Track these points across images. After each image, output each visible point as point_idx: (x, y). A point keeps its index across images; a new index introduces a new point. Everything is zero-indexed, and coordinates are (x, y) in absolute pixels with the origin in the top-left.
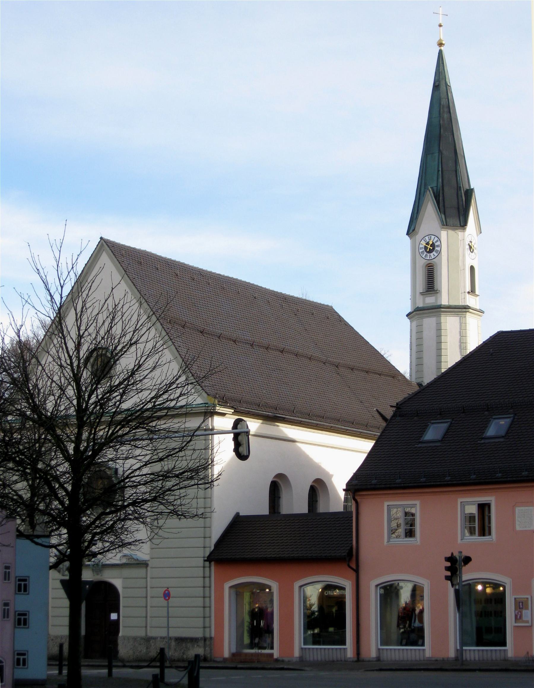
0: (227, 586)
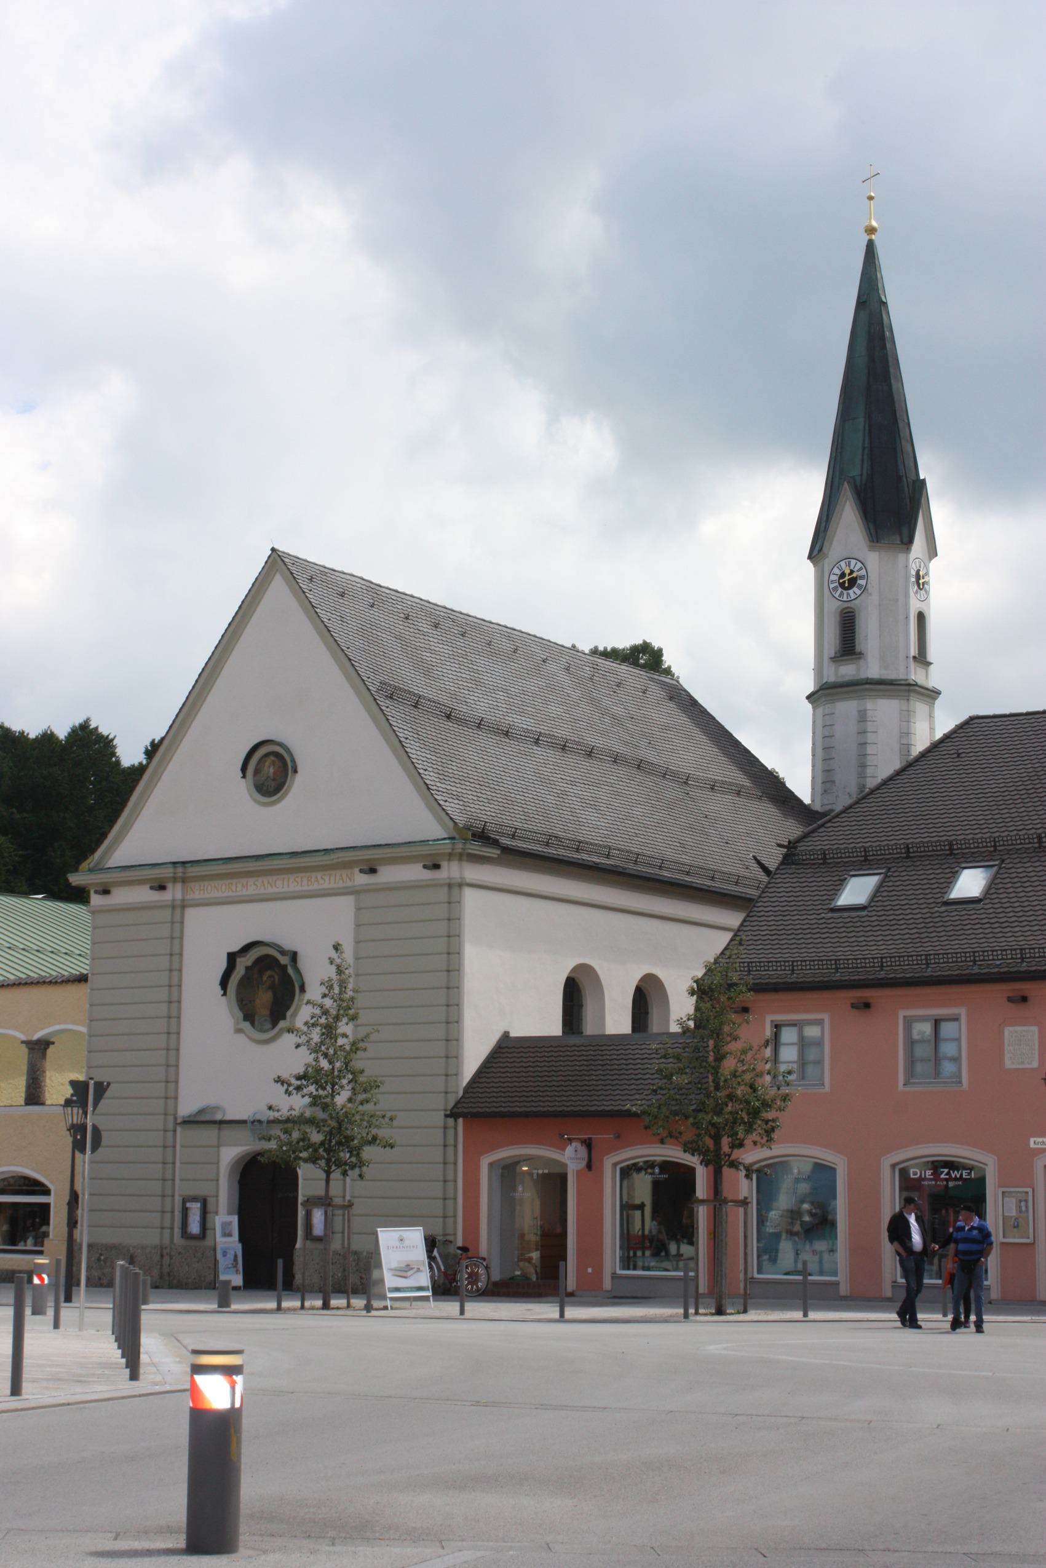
0: (485, 1162)
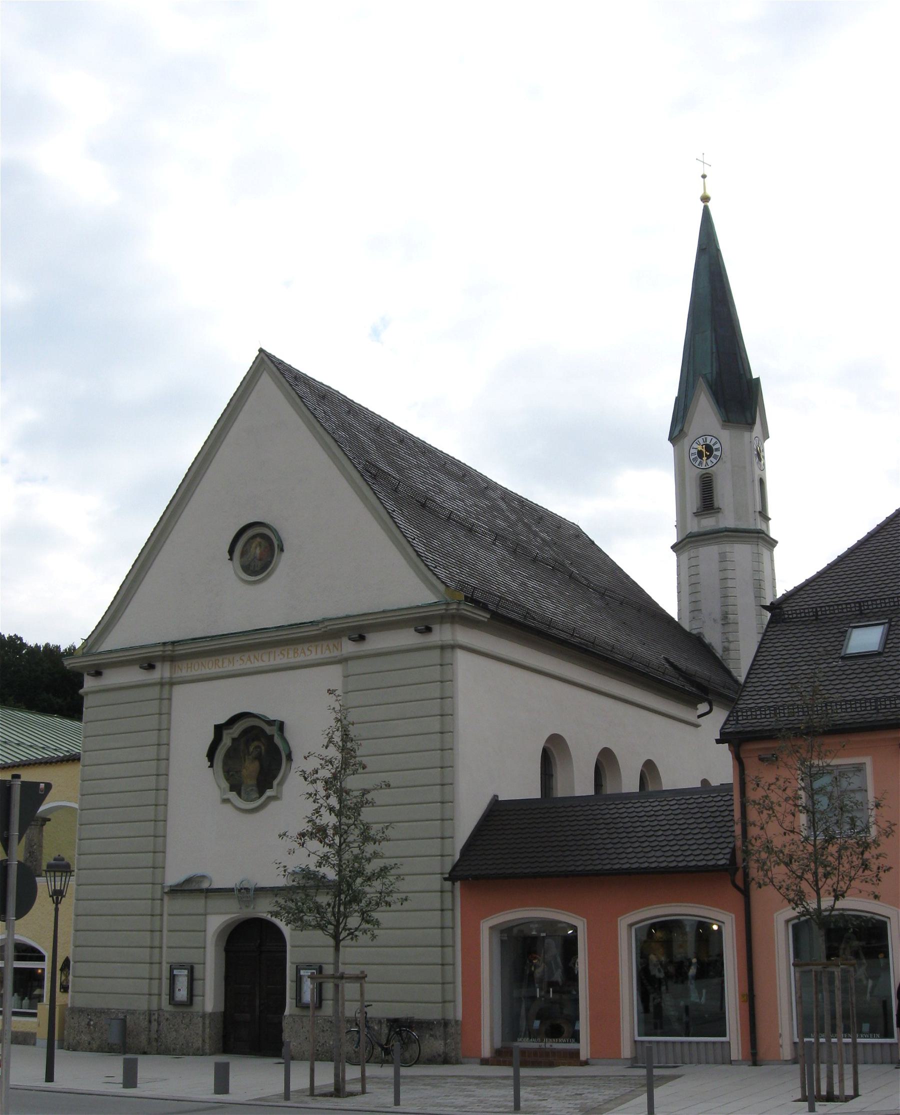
0: (485, 925)
